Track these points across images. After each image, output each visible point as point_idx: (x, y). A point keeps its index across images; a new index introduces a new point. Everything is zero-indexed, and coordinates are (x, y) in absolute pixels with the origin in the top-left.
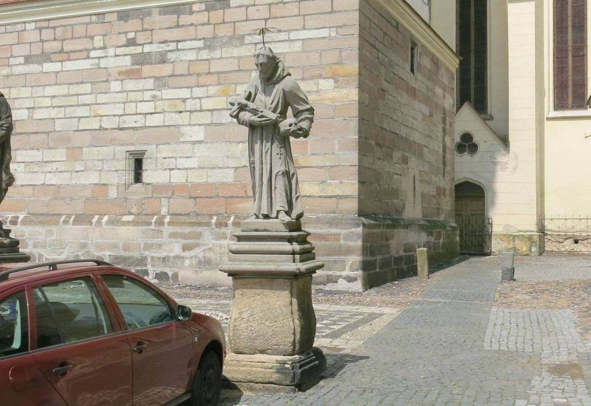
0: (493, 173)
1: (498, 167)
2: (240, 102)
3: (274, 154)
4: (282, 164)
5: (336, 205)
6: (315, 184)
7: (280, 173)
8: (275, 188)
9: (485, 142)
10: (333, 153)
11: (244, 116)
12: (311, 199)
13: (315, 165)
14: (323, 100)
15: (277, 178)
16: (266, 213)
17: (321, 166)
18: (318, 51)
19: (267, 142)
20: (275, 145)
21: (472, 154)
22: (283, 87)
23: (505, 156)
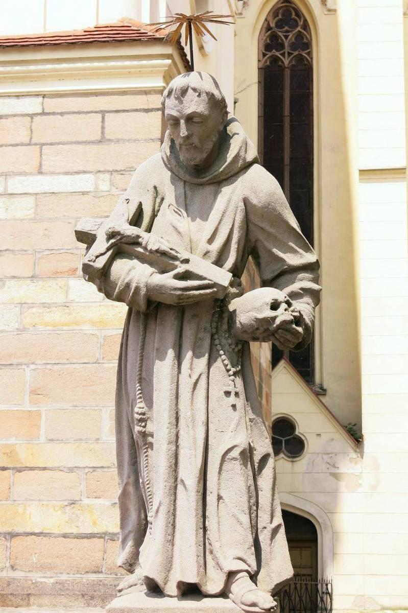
0: (334, 494)
1: (343, 485)
2: (118, 229)
3: (217, 392)
4: (238, 424)
5: (100, 554)
6: (54, 507)
7: (236, 453)
8: (220, 498)
9: (319, 435)
10: (98, 439)
11: (128, 273)
12: (45, 540)
13: (56, 464)
14: (77, 323)
15: (224, 468)
16: (192, 579)
17: (69, 468)
18: (70, 221)
19: (197, 355)
20: (218, 365)
21: (294, 457)
22: (247, 193)
23: (356, 463)
